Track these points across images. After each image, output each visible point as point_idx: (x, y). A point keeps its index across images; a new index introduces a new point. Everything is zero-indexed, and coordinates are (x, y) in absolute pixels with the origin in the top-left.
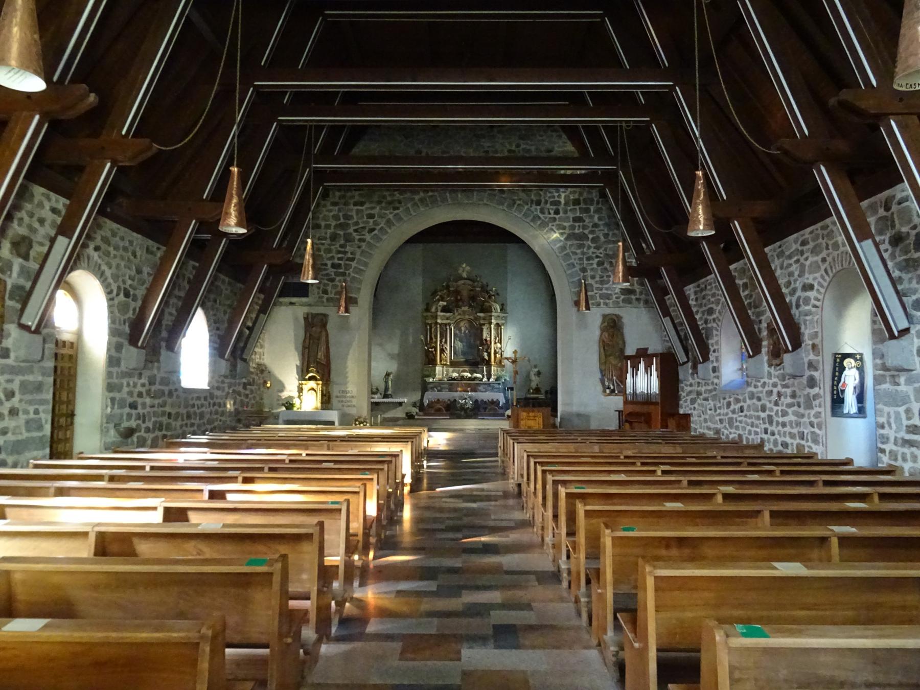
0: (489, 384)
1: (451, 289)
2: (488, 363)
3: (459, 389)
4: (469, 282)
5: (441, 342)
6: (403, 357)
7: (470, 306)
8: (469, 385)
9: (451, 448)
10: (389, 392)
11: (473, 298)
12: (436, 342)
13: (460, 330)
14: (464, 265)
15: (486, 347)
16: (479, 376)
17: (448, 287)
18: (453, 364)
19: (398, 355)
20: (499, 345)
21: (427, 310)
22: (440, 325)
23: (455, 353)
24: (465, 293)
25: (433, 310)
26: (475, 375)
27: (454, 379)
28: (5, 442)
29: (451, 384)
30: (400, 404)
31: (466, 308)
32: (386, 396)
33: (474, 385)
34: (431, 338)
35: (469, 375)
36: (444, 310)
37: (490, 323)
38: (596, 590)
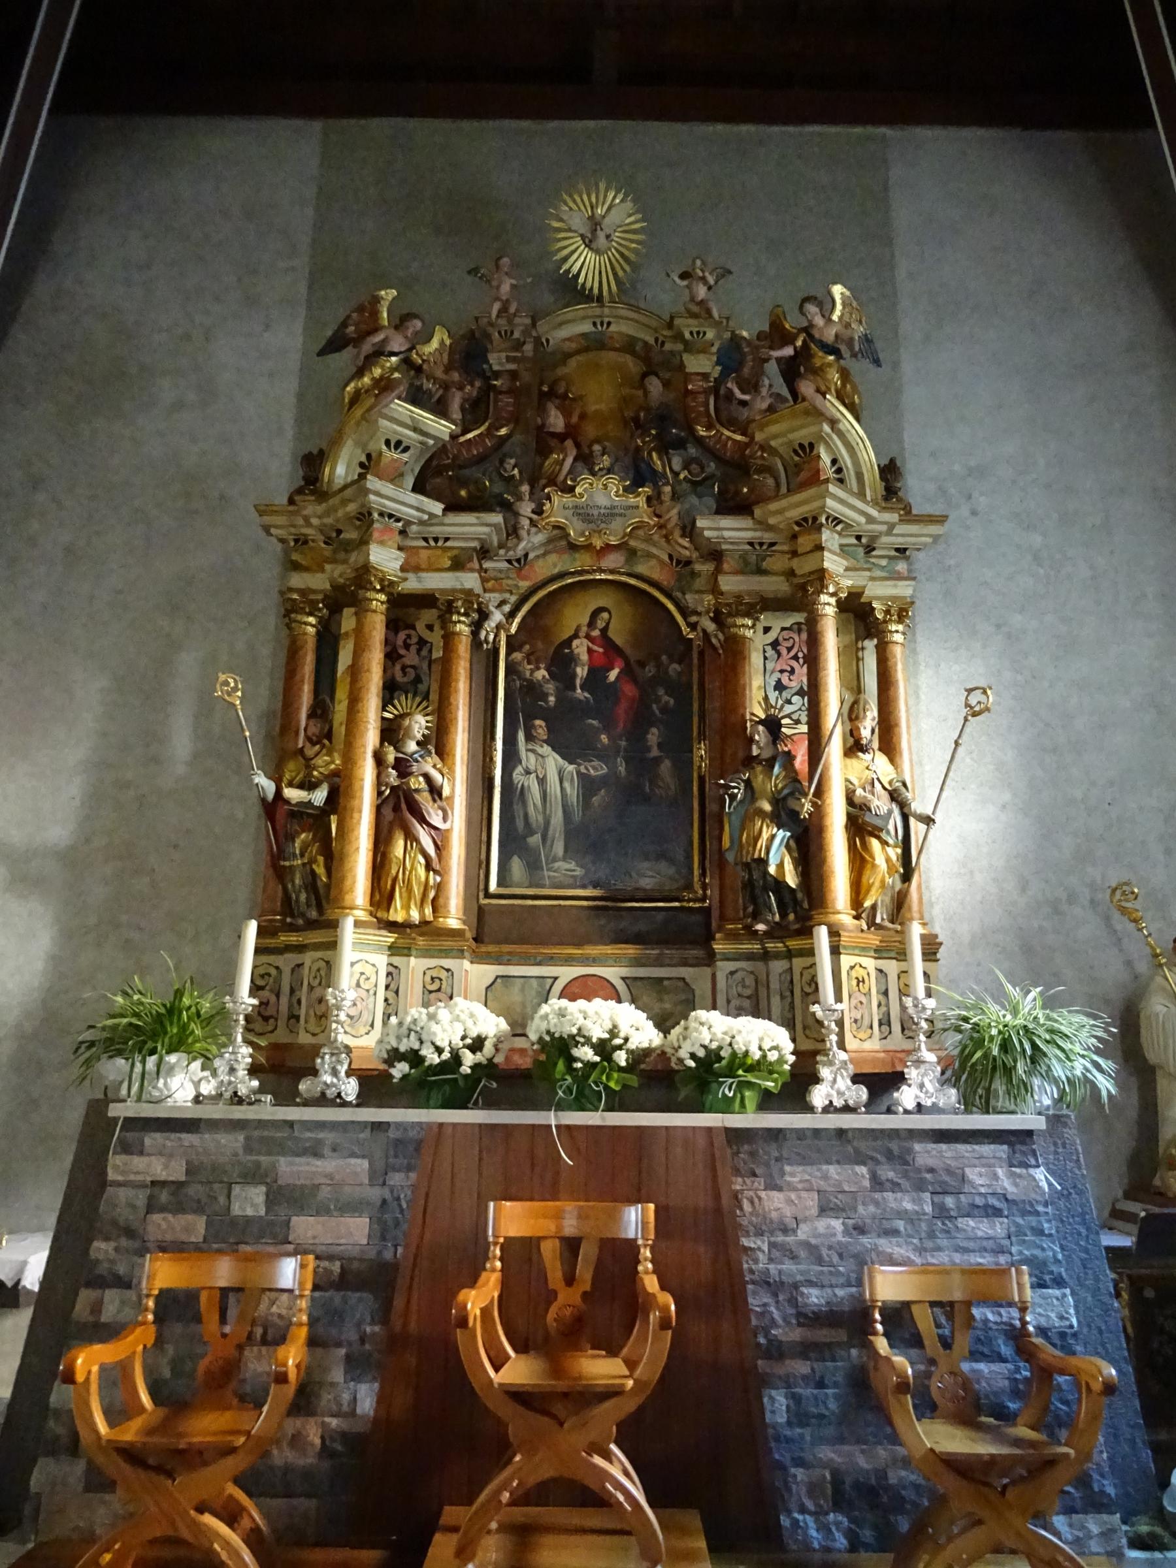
0: (893, 1147)
2: (807, 902)
5: (391, 732)
7: (639, 476)
9: (569, 1354)
13: (561, 663)
16: (763, 1037)
18: (495, 930)
19: (72, 859)
22: (404, 608)
23: (512, 842)
25: (341, 470)
27: (439, 1081)
31: (603, 491)
34: (321, 711)
35: (638, 1030)
36: (439, 475)
37: (800, 597)
38: (779, 1233)
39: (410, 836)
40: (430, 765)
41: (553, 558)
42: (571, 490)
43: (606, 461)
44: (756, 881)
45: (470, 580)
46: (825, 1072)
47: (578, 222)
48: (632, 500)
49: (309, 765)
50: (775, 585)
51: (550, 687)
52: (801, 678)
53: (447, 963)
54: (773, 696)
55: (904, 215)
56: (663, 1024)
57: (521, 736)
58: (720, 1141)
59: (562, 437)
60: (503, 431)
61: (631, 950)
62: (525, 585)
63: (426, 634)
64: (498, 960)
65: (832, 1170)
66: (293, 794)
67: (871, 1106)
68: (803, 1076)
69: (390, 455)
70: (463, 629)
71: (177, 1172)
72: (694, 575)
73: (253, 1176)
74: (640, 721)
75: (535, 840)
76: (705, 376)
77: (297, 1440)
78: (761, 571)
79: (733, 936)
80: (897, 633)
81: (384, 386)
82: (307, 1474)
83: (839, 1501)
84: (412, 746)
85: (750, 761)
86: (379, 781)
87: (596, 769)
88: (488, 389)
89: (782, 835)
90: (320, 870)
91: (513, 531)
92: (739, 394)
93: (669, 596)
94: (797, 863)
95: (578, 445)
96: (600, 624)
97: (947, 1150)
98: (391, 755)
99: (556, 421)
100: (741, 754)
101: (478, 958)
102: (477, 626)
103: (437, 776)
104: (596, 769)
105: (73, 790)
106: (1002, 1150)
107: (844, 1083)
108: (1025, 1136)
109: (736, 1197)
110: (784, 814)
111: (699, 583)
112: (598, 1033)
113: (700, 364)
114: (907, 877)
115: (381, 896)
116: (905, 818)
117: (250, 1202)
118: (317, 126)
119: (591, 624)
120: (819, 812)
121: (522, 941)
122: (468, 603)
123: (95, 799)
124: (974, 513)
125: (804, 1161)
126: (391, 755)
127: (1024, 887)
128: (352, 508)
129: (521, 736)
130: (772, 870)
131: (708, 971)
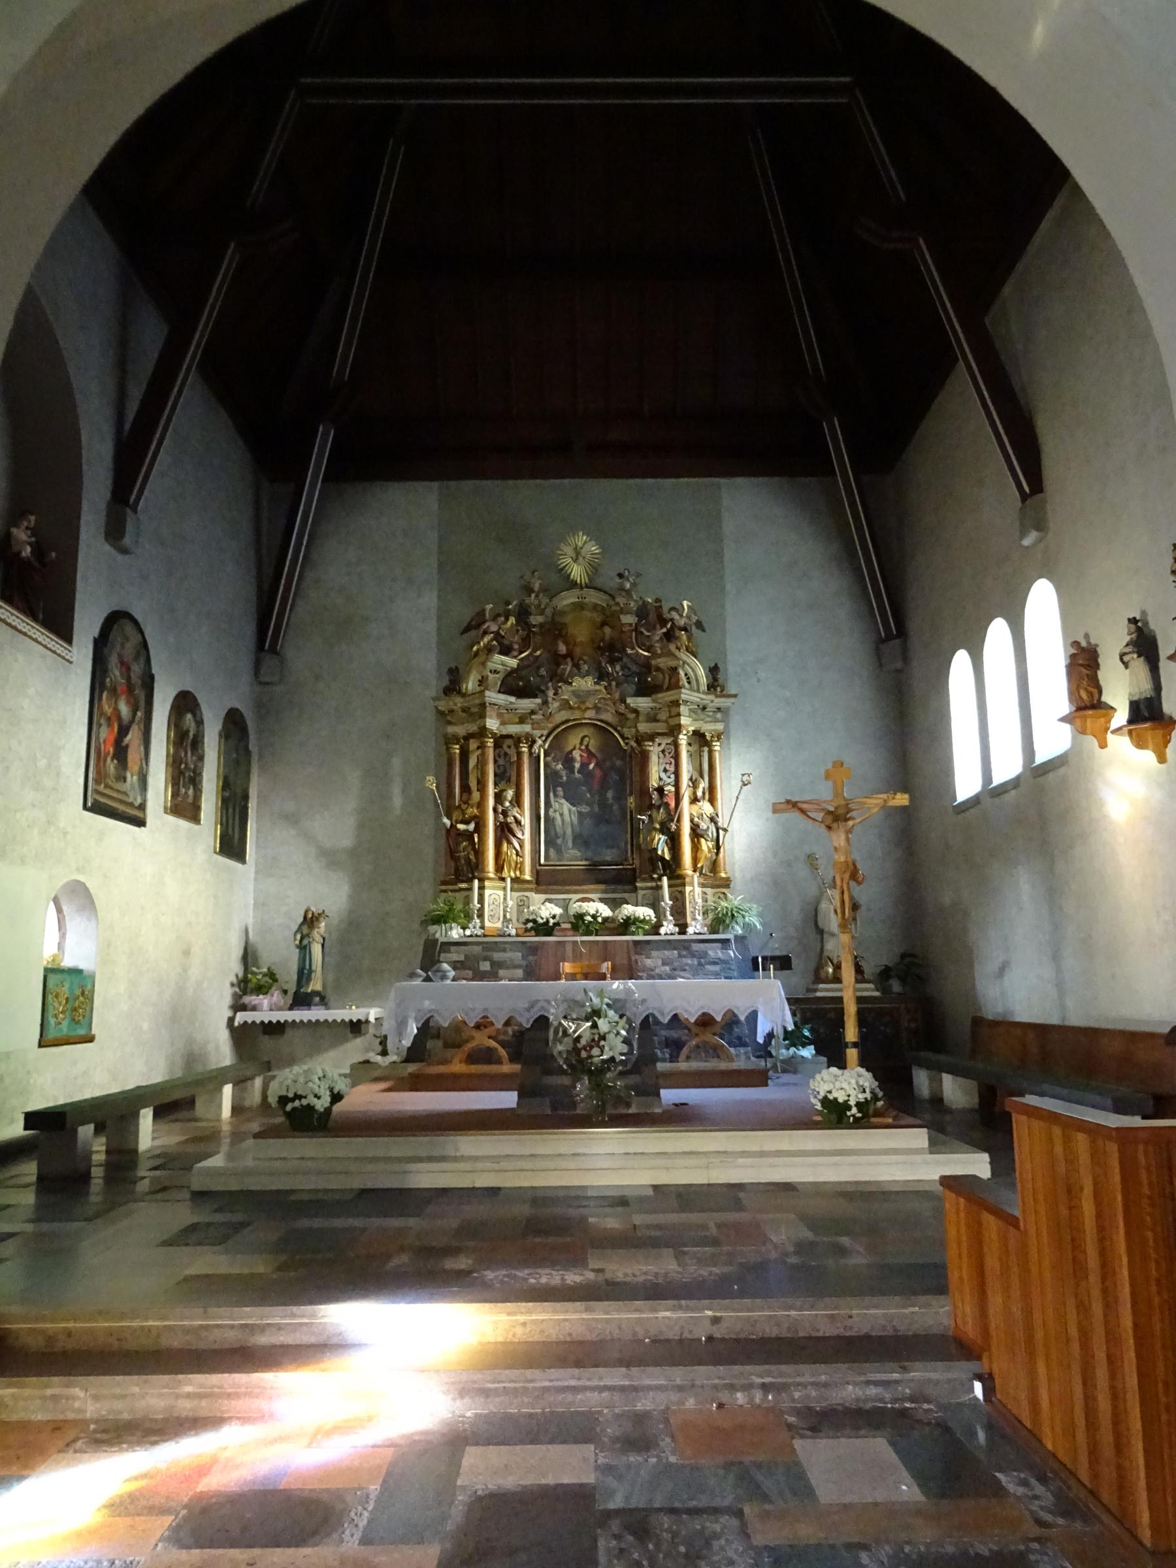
0: (684, 947)
1: (536, 620)
2: (672, 868)
3: (567, 967)
4: (593, 597)
5: (499, 798)
6: (369, 862)
7: (602, 676)
8: (605, 951)
10: (315, 985)
11: (611, 650)
12: (481, 805)
13: (568, 761)
14: (581, 539)
15: (661, 814)
17: (523, 614)
19: (353, 853)
20: (707, 808)
21: (453, 687)
22: (499, 740)
24: (581, 632)
25: (470, 685)
26: (628, 910)
27: (544, 929)
28: (466, 956)
29: (534, 949)
30: (356, 1027)
31: (585, 683)
32: (301, 1000)
33: (625, 952)
34: (465, 788)
35: (605, 911)
36: (514, 685)
37: (674, 730)
39: (510, 843)
40: (515, 812)
41: (563, 712)
42: (570, 684)
43: (586, 667)
44: (653, 858)
45: (527, 728)
46: (665, 923)
47: (569, 551)
48: (598, 687)
49: (464, 813)
50: (660, 727)
51: (564, 773)
52: (672, 769)
53: (526, 894)
54: (663, 775)
55: (729, 527)
56: (613, 911)
57: (551, 795)
58: (631, 945)
59: (565, 657)
60: (538, 653)
61: (602, 887)
62: (550, 726)
63: (508, 750)
64: (546, 893)
65: (666, 952)
66: (461, 827)
67: (679, 933)
68: (658, 925)
69: (491, 676)
70: (525, 750)
71: (462, 958)
72: (627, 719)
73: (485, 959)
74: (604, 786)
75: (559, 841)
76: (631, 625)
77: (505, 1033)
78: (656, 720)
79: (644, 880)
80: (717, 746)
81: (489, 650)
82: (508, 1042)
83: (667, 1046)
84: (507, 804)
85: (651, 806)
86: (496, 819)
87: (585, 809)
88: (530, 631)
89: (663, 838)
90: (472, 857)
91: (545, 703)
92: (647, 634)
93: (616, 730)
94: (670, 850)
95: (572, 660)
96: (585, 743)
97: (702, 946)
98: (500, 809)
99: (562, 649)
100: (647, 803)
101: (537, 892)
102: (530, 747)
103: (518, 816)
104: (585, 809)
105: (350, 822)
106: (719, 945)
107: (671, 926)
108: (728, 940)
109: (636, 961)
110: (664, 829)
111: (629, 723)
112: (592, 912)
113: (629, 619)
114: (717, 854)
115: (499, 868)
116: (717, 830)
117: (485, 966)
118: (435, 485)
119: (581, 743)
120: (679, 829)
121: (556, 884)
122: (527, 739)
123: (361, 826)
124: (759, 680)
125: (658, 950)
126: (500, 809)
127: (775, 855)
128: (477, 701)
129: (551, 795)
130: (660, 852)
131: (633, 895)
